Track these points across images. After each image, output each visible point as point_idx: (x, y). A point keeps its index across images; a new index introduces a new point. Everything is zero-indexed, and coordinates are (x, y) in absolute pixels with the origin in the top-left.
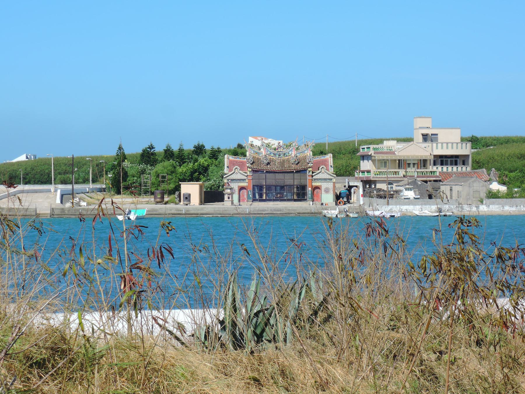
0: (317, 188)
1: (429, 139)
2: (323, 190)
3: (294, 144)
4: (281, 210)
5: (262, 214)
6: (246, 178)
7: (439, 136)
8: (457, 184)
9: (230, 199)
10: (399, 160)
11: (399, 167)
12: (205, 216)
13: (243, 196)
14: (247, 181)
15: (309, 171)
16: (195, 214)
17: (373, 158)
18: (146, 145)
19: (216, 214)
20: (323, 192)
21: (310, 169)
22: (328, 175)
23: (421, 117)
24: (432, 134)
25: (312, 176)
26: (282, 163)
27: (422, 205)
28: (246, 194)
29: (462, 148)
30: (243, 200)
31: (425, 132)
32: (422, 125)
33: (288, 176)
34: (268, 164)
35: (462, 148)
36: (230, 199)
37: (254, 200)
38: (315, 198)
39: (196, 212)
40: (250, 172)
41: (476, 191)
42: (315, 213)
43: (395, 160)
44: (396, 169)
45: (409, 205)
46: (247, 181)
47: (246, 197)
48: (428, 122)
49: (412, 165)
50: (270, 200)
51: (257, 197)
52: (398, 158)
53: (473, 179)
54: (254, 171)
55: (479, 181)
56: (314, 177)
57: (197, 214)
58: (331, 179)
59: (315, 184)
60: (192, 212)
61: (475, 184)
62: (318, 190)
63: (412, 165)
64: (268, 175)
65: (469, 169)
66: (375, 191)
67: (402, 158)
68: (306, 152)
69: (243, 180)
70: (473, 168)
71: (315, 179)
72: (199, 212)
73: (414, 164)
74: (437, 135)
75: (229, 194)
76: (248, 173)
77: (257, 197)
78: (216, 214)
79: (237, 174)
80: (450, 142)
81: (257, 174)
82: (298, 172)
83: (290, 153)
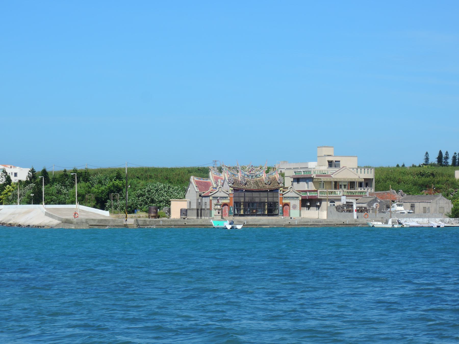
0: (287, 204)
1: (333, 165)
2: (291, 207)
3: (264, 168)
4: (320, 222)
5: (308, 225)
6: (228, 196)
7: (341, 163)
8: (422, 201)
9: (220, 214)
10: (335, 182)
11: (351, 188)
12: (264, 227)
13: (225, 211)
14: (229, 198)
15: (281, 191)
16: (255, 225)
17: (314, 180)
18: (43, 169)
19: (271, 225)
20: (291, 208)
21: (282, 189)
22: (295, 194)
23: (325, 147)
24: (335, 161)
25: (283, 195)
26: (256, 183)
27: (429, 217)
28: (227, 209)
29: (361, 173)
30: (225, 215)
31: (330, 159)
32: (328, 152)
33: (263, 194)
34: (245, 184)
35: (361, 173)
36: (220, 214)
37: (235, 215)
38: (284, 213)
39: (253, 223)
40: (232, 190)
41: (442, 207)
42: (349, 224)
43: (331, 182)
44: (331, 189)
45: (419, 218)
46: (229, 198)
47: (227, 212)
48: (330, 151)
49: (343, 187)
50: (248, 215)
51: (236, 212)
52: (335, 180)
53: (439, 198)
54: (235, 190)
55: (443, 199)
56: (284, 196)
57: (257, 225)
58: (298, 197)
59: (285, 201)
60: (251, 223)
61: (441, 202)
62: (287, 206)
63: (343, 187)
64: (246, 193)
65: (373, 190)
66: (345, 208)
67: (338, 180)
68: (274, 174)
69: (226, 197)
70: (376, 190)
71: (285, 197)
72: (258, 223)
73: (345, 186)
74: (339, 161)
75: (219, 210)
76: (230, 192)
77: (236, 212)
78: (271, 225)
79: (220, 192)
80: (350, 170)
81: (237, 193)
82: (271, 191)
83: (261, 175)
